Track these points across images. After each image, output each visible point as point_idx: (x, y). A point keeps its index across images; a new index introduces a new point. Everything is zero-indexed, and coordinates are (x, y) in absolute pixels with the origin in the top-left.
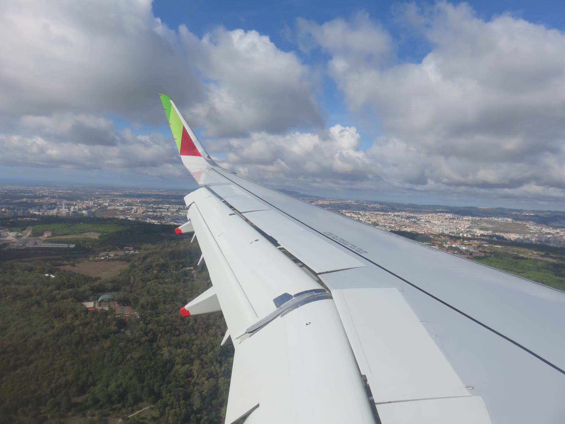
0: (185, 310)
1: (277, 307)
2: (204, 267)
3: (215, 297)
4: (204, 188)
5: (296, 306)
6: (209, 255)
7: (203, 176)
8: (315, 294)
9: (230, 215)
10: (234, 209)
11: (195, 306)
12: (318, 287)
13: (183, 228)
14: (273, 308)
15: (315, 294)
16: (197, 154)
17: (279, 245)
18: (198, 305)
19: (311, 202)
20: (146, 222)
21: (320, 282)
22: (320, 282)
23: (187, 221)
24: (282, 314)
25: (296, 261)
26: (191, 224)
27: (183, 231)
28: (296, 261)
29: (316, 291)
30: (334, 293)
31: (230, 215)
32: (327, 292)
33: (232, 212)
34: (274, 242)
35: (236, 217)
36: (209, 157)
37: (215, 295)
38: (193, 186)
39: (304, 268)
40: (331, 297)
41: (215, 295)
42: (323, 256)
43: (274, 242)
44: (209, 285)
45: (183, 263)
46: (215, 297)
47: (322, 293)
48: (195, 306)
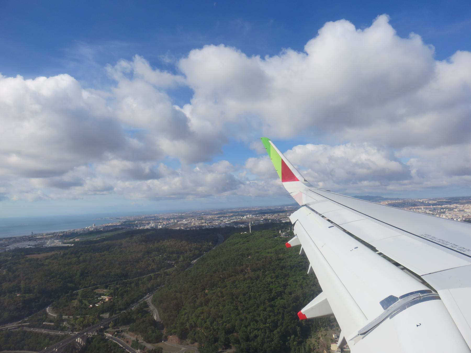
0: (301, 313)
1: (385, 309)
2: (312, 273)
3: (326, 302)
4: (305, 207)
5: (403, 308)
6: (317, 264)
7: (304, 196)
8: (421, 295)
9: (329, 227)
10: (332, 222)
11: (310, 310)
12: (424, 288)
13: (292, 242)
14: (380, 310)
15: (421, 295)
16: (297, 180)
17: (377, 251)
18: (312, 309)
19: (410, 209)
20: (314, 143)
21: (424, 282)
22: (424, 282)
23: (294, 236)
24: (391, 316)
25: (397, 264)
26: (298, 238)
27: (292, 245)
28: (397, 264)
29: (422, 292)
30: (441, 293)
31: (329, 227)
32: (433, 292)
33: (331, 225)
34: (373, 249)
35: (335, 228)
36: (305, 181)
37: (326, 299)
38: (296, 207)
39: (405, 270)
40: (439, 298)
41: (326, 299)
42: (428, 260)
43: (373, 249)
44: (320, 291)
45: (297, 278)
46: (326, 302)
47: (428, 294)
48: (310, 310)
